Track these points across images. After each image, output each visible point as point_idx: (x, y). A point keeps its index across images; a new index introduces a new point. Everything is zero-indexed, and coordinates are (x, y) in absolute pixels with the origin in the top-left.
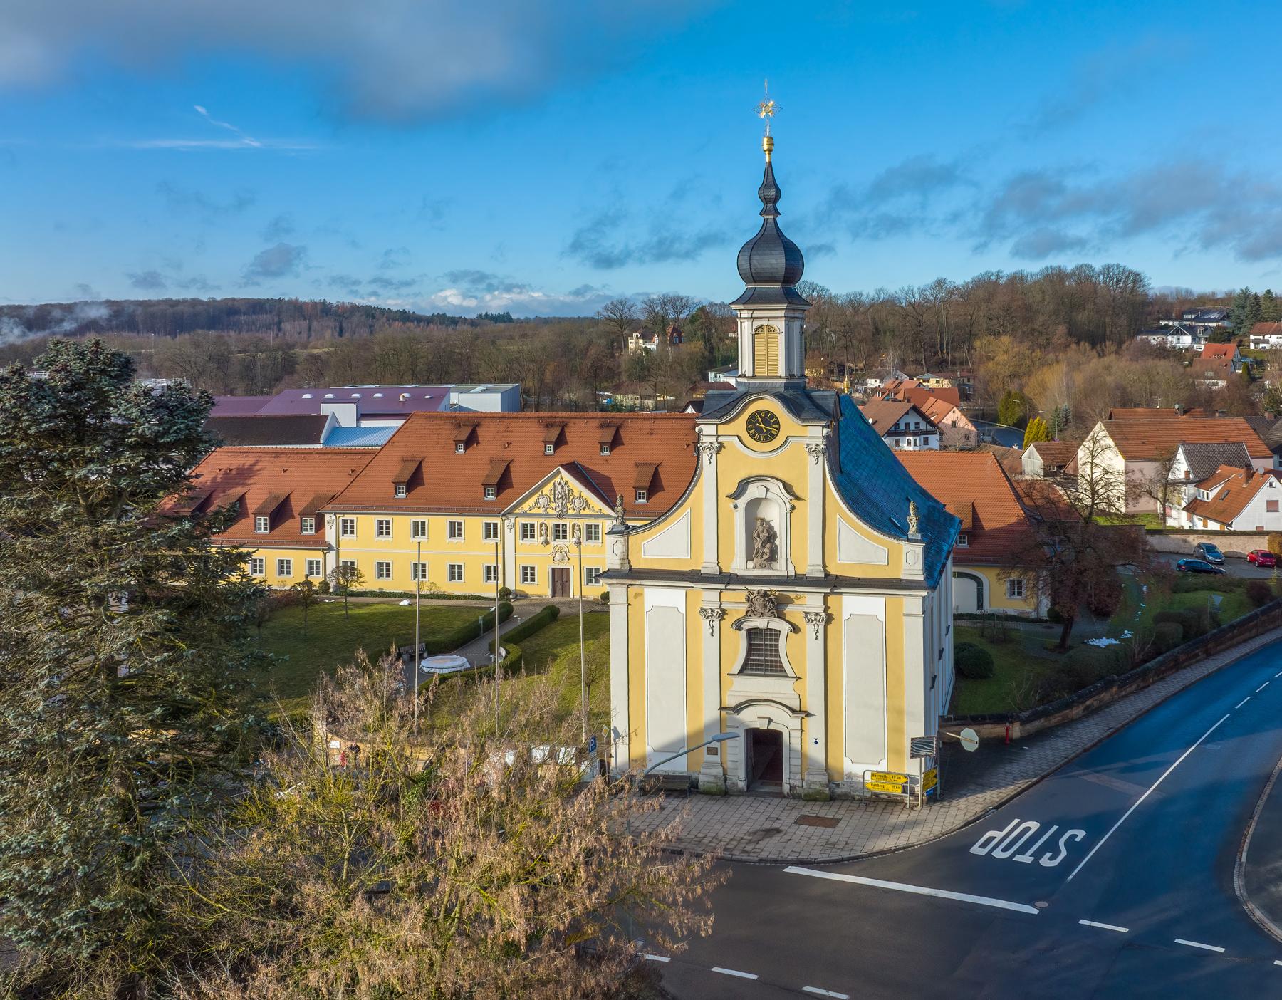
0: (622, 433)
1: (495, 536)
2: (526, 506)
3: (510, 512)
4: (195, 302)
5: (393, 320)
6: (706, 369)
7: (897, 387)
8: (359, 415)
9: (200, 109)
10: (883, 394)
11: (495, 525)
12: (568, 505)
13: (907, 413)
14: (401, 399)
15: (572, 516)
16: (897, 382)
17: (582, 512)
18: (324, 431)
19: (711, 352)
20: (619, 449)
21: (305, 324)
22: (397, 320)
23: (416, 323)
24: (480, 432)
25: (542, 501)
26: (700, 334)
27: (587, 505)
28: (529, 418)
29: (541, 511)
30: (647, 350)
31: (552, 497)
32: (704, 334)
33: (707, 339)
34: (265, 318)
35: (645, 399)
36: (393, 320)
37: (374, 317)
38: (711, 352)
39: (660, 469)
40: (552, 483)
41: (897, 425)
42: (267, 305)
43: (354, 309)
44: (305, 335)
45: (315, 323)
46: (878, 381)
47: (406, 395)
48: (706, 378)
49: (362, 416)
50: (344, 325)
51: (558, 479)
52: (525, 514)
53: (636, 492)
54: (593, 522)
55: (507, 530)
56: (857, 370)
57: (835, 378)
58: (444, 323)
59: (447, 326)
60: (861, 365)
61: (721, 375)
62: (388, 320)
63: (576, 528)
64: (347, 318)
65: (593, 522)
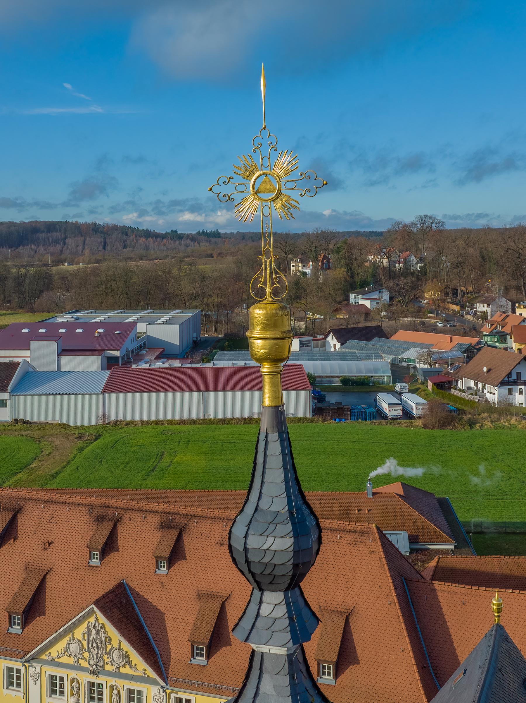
0: (187, 540)
1: (19, 685)
2: (54, 651)
3: (34, 658)
4: (12, 224)
5: (140, 236)
6: (348, 291)
7: (504, 320)
8: (60, 351)
9: (68, 86)
10: (492, 325)
11: (18, 671)
12: (105, 657)
13: (519, 363)
14: (96, 335)
15: (109, 674)
16: (504, 315)
17: (122, 670)
18: (13, 380)
19: (352, 277)
20: (179, 565)
21: (81, 239)
22: (142, 236)
23: (154, 238)
24: (21, 520)
25: (73, 647)
26: (343, 262)
27: (128, 661)
28: (79, 504)
29: (71, 661)
30: (305, 274)
31: (85, 643)
32: (346, 262)
33: (349, 267)
34: (56, 235)
35: (298, 321)
36: (140, 236)
37: (127, 235)
38: (352, 277)
39: (228, 606)
40: (85, 625)
41: (509, 375)
42: (58, 226)
43: (115, 228)
44: (80, 248)
45: (88, 239)
46: (486, 305)
47: (101, 330)
48: (347, 299)
49: (63, 351)
50: (107, 240)
51: (92, 620)
52: (53, 663)
53: (192, 646)
54: (136, 686)
55: (31, 682)
56: (468, 293)
57: (450, 300)
58: (174, 239)
59: (175, 241)
60: (470, 289)
61: (360, 297)
62: (136, 236)
63: (115, 692)
64: (110, 235)
65: (136, 686)
